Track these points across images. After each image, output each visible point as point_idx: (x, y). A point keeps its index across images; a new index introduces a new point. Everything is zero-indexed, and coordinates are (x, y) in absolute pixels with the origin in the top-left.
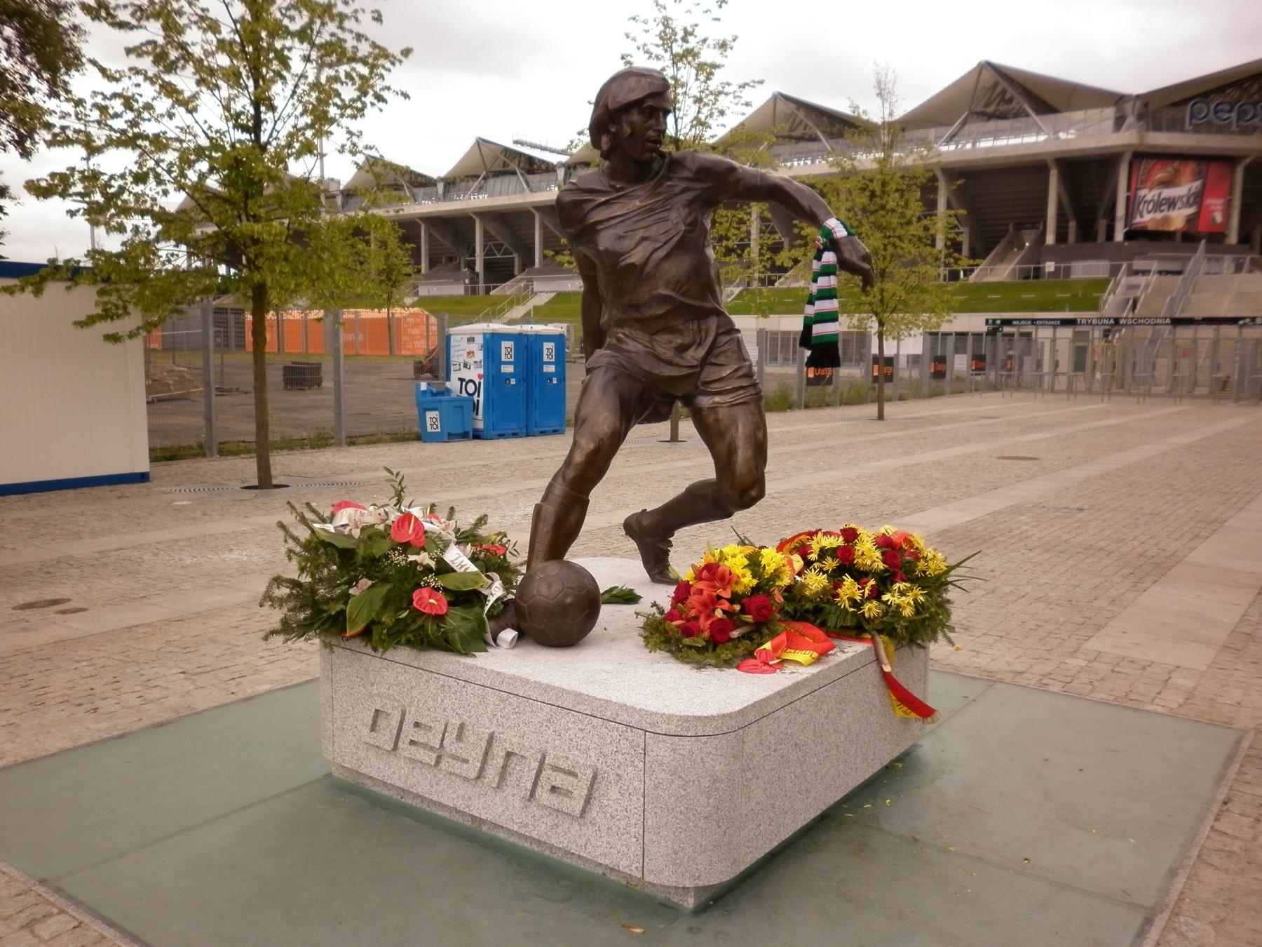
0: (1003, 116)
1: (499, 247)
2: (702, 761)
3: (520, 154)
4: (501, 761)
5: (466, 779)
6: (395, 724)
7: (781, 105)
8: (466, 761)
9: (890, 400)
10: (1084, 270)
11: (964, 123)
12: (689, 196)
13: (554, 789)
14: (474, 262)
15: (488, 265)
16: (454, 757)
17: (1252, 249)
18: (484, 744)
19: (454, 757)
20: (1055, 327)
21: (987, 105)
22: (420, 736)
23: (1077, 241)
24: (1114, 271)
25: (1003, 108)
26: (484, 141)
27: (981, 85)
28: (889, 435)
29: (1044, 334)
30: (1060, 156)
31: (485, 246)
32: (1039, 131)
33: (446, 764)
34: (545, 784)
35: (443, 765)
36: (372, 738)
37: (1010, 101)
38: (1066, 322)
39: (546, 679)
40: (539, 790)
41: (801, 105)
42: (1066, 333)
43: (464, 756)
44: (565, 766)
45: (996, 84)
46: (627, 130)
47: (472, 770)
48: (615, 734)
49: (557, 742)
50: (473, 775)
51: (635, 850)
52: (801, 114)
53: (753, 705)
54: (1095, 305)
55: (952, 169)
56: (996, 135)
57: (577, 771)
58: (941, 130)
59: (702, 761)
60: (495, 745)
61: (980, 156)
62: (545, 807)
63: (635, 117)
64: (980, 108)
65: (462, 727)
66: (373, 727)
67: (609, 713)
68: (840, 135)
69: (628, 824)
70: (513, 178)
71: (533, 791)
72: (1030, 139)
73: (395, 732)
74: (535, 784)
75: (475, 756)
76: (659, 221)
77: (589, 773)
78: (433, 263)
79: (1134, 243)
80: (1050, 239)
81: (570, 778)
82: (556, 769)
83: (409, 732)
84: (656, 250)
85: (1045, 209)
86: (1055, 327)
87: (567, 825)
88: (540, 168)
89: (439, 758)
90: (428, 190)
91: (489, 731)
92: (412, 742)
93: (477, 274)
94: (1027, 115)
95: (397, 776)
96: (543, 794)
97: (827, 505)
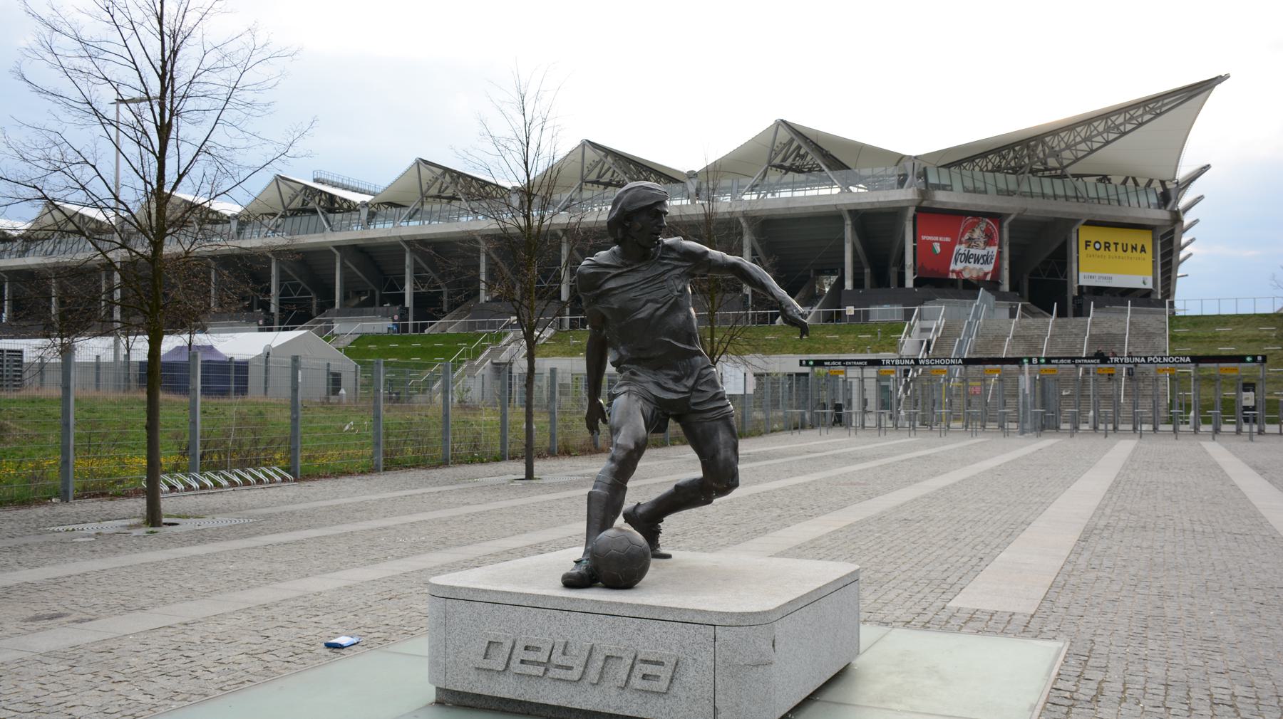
0: (799, 170)
1: (296, 287)
3: (322, 192)
4: (601, 664)
7: (591, 155)
8: (570, 668)
9: (759, 431)
10: (883, 312)
14: (268, 304)
18: (586, 654)
20: (862, 367)
21: (784, 160)
22: (531, 656)
23: (872, 287)
24: (908, 315)
27: (777, 143)
29: (853, 373)
30: (852, 208)
31: (281, 286)
32: (832, 184)
33: (554, 673)
37: (803, 157)
38: (872, 363)
39: (640, 602)
41: (608, 152)
42: (871, 372)
43: (569, 664)
44: (654, 659)
45: (792, 141)
46: (639, 225)
54: (894, 346)
56: (794, 186)
58: (743, 181)
61: (781, 205)
70: (314, 218)
72: (825, 191)
74: (629, 676)
80: (849, 285)
82: (646, 662)
85: (843, 257)
86: (862, 367)
88: (341, 206)
89: (546, 670)
90: (219, 228)
94: (821, 170)
96: (637, 682)
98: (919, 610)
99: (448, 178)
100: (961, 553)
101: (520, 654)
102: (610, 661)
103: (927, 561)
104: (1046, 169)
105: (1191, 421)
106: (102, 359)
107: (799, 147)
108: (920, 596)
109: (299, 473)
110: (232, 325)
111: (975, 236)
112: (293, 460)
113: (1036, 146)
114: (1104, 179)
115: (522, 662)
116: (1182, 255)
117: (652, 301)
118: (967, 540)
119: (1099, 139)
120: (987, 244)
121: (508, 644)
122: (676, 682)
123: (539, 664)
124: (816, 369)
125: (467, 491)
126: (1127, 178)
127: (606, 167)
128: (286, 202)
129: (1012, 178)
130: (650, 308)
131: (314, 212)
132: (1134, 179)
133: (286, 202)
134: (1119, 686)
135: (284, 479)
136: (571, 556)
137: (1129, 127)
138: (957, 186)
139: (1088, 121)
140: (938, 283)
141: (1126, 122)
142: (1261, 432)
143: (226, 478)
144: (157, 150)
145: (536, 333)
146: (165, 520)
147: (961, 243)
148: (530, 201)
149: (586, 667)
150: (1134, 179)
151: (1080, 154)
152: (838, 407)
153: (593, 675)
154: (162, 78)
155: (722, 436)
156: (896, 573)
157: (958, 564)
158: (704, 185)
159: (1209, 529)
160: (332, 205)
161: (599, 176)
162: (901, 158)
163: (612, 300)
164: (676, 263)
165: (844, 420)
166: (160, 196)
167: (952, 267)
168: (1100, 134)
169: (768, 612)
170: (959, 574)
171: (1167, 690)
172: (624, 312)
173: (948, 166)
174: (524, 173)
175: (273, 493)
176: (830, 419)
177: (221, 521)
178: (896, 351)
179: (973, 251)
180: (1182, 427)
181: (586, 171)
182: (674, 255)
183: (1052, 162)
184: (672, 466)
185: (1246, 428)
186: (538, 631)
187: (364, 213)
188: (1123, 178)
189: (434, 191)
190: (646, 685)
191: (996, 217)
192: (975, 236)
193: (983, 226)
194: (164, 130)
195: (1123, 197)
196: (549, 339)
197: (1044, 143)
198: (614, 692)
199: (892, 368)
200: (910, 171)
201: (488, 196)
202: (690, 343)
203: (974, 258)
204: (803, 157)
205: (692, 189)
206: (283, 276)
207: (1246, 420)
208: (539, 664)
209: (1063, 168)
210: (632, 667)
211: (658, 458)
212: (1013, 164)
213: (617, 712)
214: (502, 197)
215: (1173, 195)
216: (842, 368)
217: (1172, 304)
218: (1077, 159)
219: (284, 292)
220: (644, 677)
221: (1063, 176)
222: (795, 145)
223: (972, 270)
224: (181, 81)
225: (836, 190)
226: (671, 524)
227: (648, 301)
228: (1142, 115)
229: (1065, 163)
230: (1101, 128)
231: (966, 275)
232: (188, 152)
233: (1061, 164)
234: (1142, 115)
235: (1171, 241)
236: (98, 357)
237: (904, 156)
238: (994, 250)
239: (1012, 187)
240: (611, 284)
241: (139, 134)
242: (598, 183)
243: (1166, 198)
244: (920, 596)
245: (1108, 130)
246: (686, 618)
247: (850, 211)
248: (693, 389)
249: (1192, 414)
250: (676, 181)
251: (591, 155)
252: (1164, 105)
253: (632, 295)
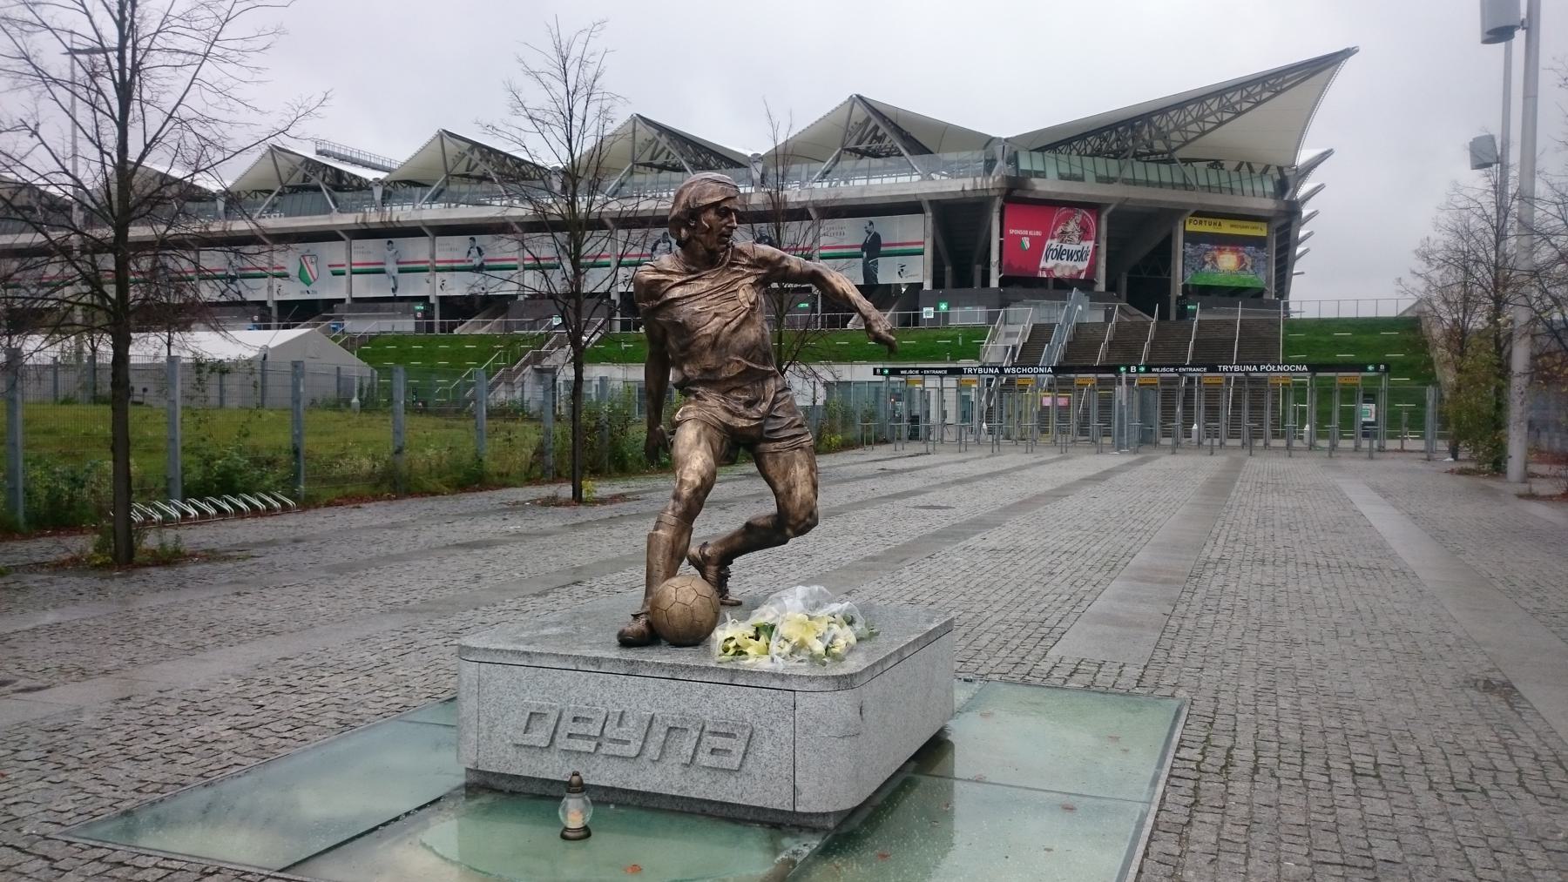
0: (876, 155)
4: (662, 737)
8: (627, 742)
11: (838, 159)
12: (752, 280)
17: (1119, 297)
20: (942, 376)
21: (859, 143)
22: (580, 728)
24: (992, 318)
25: (875, 145)
28: (50, 617)
29: (931, 383)
37: (880, 139)
42: (951, 382)
45: (868, 120)
51: (788, 789)
52: (664, 140)
54: (976, 355)
55: (826, 208)
58: (814, 166)
63: (711, 215)
64: (852, 145)
70: (318, 195)
74: (695, 751)
77: (747, 733)
79: (1009, 290)
82: (715, 733)
88: (350, 184)
89: (599, 745)
93: (270, 309)
94: (900, 155)
96: (704, 759)
98: (1016, 659)
99: (477, 155)
100: (1059, 590)
101: (567, 726)
102: (673, 733)
103: (1021, 599)
104: (1152, 153)
105: (1306, 436)
107: (876, 128)
108: (1017, 641)
111: (1069, 229)
113: (1142, 126)
114: (1216, 164)
115: (570, 736)
116: (1299, 250)
118: (1065, 575)
119: (1212, 119)
120: (1083, 238)
121: (553, 716)
122: (750, 758)
123: (589, 738)
124: (892, 379)
126: (1241, 164)
129: (1113, 164)
131: (318, 189)
132: (1249, 165)
133: (285, 178)
134: (1249, 754)
136: (625, 601)
137: (1246, 106)
138: (1052, 173)
139: (1200, 98)
140: (1025, 283)
141: (1243, 100)
142: (1381, 449)
144: (117, 115)
145: (585, 338)
147: (1053, 237)
148: (575, 186)
149: (645, 741)
150: (1249, 165)
151: (1191, 136)
152: (914, 419)
153: (653, 750)
154: (120, 25)
156: (988, 614)
157: (1057, 604)
158: (772, 171)
159: (1333, 563)
160: (340, 182)
161: (652, 158)
162: (991, 140)
165: (922, 433)
166: (125, 171)
167: (1043, 264)
168: (1212, 113)
170: (1058, 615)
171: (1303, 758)
173: (1041, 150)
174: (567, 152)
176: (905, 433)
178: (977, 358)
179: (1065, 246)
180: (1296, 443)
183: (1159, 145)
184: (743, 499)
185: (1365, 444)
187: (378, 193)
188: (1235, 164)
189: (461, 169)
190: (713, 761)
191: (1094, 207)
192: (1069, 229)
193: (1079, 218)
194: (125, 92)
195: (1236, 185)
197: (1151, 124)
198: (677, 770)
199: (975, 377)
200: (999, 154)
201: (524, 176)
203: (1069, 253)
204: (880, 139)
205: (756, 176)
207: (1365, 435)
208: (589, 738)
209: (1171, 151)
210: (700, 739)
212: (1114, 147)
213: (681, 794)
214: (542, 178)
215: (1291, 182)
216: (920, 377)
217: (1286, 305)
218: (1187, 142)
221: (1170, 161)
222: (871, 125)
223: (1064, 268)
224: (148, 26)
225: (916, 178)
228: (1260, 93)
229: (1174, 145)
230: (1214, 107)
231: (1058, 274)
232: (155, 119)
233: (1169, 147)
234: (1260, 93)
235: (1288, 235)
237: (992, 139)
238: (1090, 245)
239: (1113, 173)
241: (94, 95)
242: (651, 165)
243: (1283, 186)
244: (1017, 641)
245: (1222, 109)
247: (931, 202)
249: (1307, 428)
250: (739, 165)
251: (645, 133)
252: (1285, 82)
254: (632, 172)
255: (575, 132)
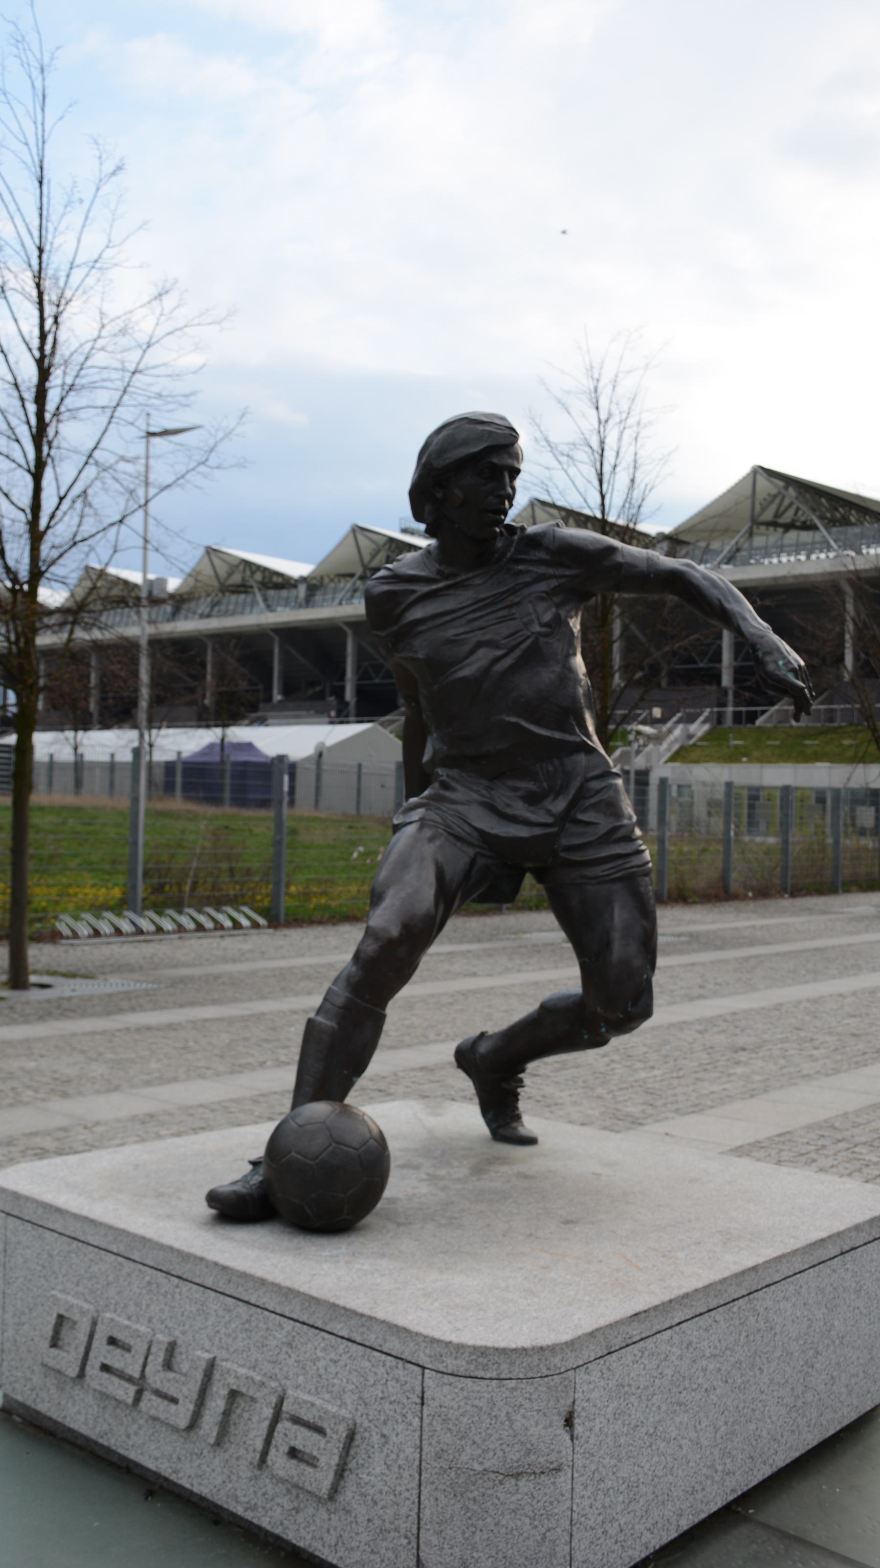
2: (509, 1419)
5: (175, 1429)
6: (83, 1338)
7: (763, 483)
8: (174, 1401)
13: (293, 1453)
14: (342, 689)
15: (360, 692)
16: (158, 1393)
19: (158, 1393)
26: (363, 529)
33: (150, 1402)
34: (280, 1445)
35: (143, 1405)
36: (55, 1358)
40: (272, 1452)
43: (172, 1392)
46: (459, 493)
47: (181, 1415)
48: (381, 1370)
49: (301, 1379)
50: (183, 1423)
52: (792, 492)
53: (592, 1334)
57: (325, 1425)
59: (509, 1419)
60: (216, 1376)
62: (282, 1481)
65: (172, 1348)
66: (55, 1342)
67: (372, 1337)
68: (845, 522)
69: (397, 1516)
71: (265, 1453)
73: (82, 1350)
75: (187, 1391)
76: (502, 620)
78: (289, 690)
81: (316, 1436)
83: (101, 1353)
84: (497, 660)
87: (311, 1511)
90: (284, 593)
91: (207, 1356)
92: (105, 1368)
93: (347, 704)
95: (82, 1418)
97: (802, 1034)
106: (56, 758)
109: (276, 918)
110: (298, 717)
112: (275, 896)
117: (491, 644)
125: (489, 954)
127: (787, 502)
128: (366, 558)
130: (484, 656)
133: (366, 558)
135: (255, 925)
136: (235, 1152)
143: (248, 917)
144: (33, 469)
146: (33, 979)
154: (40, 362)
155: (620, 915)
161: (777, 515)
163: (417, 642)
164: (542, 570)
169: (553, 1349)
172: (437, 666)
175: (233, 944)
177: (114, 984)
181: (758, 509)
182: (542, 555)
186: (132, 1309)
196: (703, 738)
202: (563, 727)
206: (361, 655)
211: (810, 911)
213: (249, 1516)
219: (362, 674)
220: (293, 1453)
226: (544, 1081)
227: (480, 645)
236: (112, 755)
240: (417, 613)
246: (371, 1339)
248: (566, 818)
251: (765, 486)
253: (450, 633)
254: (751, 534)
255: (607, 469)
